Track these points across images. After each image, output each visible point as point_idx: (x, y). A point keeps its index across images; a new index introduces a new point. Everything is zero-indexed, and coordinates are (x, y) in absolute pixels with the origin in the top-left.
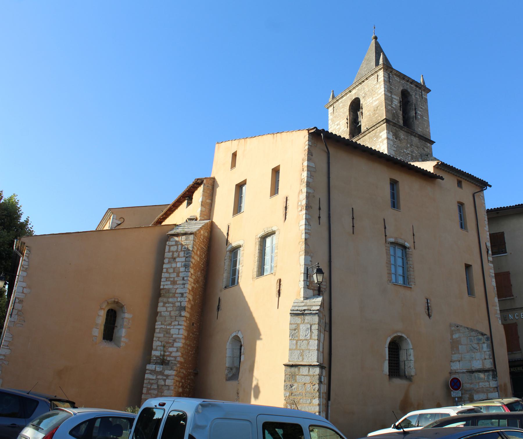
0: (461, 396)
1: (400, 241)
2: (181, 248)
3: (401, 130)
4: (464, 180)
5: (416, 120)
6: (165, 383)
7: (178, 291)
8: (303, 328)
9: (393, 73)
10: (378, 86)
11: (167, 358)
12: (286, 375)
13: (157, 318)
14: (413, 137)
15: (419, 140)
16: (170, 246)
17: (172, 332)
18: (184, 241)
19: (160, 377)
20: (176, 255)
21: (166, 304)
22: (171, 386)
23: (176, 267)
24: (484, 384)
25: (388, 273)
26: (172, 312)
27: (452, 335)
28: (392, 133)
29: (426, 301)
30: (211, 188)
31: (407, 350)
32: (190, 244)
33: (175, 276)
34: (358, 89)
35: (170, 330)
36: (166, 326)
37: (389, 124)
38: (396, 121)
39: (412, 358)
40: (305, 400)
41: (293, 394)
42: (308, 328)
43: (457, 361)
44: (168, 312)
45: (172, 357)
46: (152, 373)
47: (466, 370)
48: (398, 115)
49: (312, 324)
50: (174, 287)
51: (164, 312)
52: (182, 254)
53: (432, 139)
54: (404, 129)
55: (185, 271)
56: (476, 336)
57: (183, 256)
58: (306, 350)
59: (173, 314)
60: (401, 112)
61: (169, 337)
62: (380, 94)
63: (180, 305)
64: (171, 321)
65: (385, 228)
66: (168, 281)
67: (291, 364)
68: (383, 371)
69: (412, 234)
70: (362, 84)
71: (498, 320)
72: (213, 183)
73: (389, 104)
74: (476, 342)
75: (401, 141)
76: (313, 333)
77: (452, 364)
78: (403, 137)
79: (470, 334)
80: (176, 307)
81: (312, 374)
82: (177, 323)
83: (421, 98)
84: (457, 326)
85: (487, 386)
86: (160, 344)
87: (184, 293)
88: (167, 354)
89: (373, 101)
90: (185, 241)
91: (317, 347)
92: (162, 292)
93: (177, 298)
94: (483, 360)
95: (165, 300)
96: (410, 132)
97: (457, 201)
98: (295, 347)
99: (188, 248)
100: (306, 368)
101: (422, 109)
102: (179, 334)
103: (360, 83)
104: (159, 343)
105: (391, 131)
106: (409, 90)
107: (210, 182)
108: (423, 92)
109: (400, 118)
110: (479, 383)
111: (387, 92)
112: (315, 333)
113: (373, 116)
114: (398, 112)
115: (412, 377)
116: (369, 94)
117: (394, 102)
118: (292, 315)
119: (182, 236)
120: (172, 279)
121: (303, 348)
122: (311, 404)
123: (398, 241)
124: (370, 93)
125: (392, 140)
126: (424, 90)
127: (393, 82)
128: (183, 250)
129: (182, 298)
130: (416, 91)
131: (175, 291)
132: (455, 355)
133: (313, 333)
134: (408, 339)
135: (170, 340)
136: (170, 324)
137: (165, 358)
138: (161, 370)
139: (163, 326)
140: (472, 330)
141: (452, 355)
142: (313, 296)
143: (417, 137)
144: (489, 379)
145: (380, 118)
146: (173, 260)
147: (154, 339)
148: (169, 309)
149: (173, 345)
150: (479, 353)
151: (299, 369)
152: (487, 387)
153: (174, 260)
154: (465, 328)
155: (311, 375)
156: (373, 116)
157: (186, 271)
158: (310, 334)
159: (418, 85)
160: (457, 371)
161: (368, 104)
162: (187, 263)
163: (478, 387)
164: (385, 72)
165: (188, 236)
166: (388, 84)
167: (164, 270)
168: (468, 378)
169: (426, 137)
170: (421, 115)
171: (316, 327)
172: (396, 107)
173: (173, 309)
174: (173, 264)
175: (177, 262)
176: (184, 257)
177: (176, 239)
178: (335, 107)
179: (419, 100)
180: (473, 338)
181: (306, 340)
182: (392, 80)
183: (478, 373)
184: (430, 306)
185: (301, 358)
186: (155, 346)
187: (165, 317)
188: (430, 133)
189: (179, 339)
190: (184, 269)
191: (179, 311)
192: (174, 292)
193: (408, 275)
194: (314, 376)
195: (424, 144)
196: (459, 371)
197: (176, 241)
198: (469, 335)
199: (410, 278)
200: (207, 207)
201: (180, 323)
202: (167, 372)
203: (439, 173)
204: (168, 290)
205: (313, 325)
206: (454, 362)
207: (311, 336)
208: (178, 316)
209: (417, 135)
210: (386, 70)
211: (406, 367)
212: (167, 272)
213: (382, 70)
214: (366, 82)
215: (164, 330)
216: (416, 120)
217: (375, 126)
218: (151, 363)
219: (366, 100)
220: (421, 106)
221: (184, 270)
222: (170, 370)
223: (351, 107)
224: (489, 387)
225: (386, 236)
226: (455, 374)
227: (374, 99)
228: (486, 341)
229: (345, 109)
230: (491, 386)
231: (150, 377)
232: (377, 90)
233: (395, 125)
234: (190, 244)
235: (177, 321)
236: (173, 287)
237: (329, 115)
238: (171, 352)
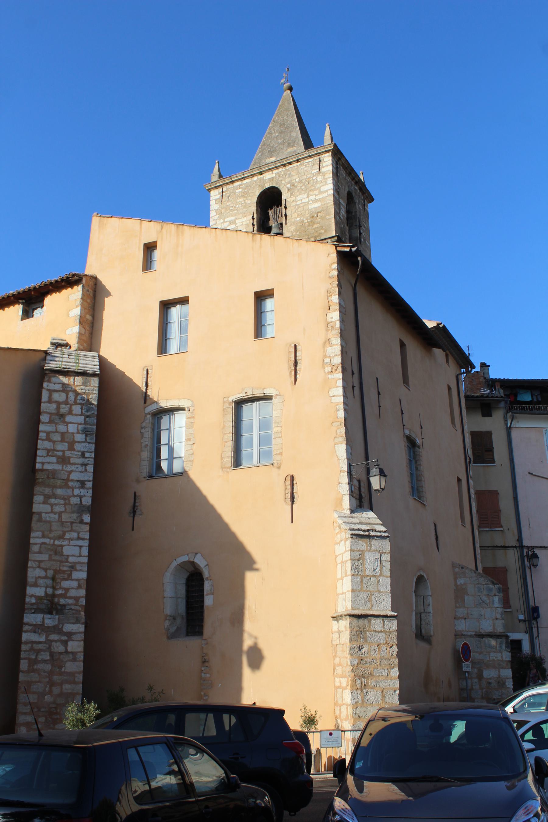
2: (75, 399)
6: (66, 648)
7: (73, 476)
8: (370, 557)
10: (320, 178)
11: (59, 600)
12: (351, 631)
13: (34, 525)
16: (51, 392)
17: (66, 551)
18: (79, 386)
19: (53, 637)
20: (64, 409)
21: (50, 500)
22: (79, 654)
23: (66, 431)
24: (496, 656)
26: (63, 514)
27: (455, 579)
30: (91, 295)
32: (93, 394)
33: (67, 449)
34: (278, 173)
35: (62, 549)
36: (52, 541)
40: (380, 671)
41: (363, 662)
43: (462, 618)
44: (55, 513)
45: (70, 598)
46: (37, 630)
47: (474, 633)
49: (382, 553)
50: (64, 469)
51: (46, 513)
52: (77, 409)
55: (86, 441)
56: (486, 584)
57: (80, 413)
58: (376, 592)
59: (65, 517)
61: (61, 562)
62: (324, 192)
63: (79, 503)
64: (63, 531)
66: (52, 456)
67: (360, 614)
70: (287, 167)
76: (384, 566)
80: (71, 506)
82: (75, 535)
84: (462, 568)
86: (42, 573)
87: (86, 481)
88: (59, 592)
89: (309, 201)
90: (81, 387)
91: (390, 588)
92: (39, 475)
93: (73, 489)
94: (494, 619)
95: (48, 491)
98: (360, 586)
99: (88, 400)
100: (380, 620)
102: (80, 556)
103: (283, 165)
104: (40, 573)
110: (489, 652)
112: (387, 566)
113: (309, 226)
116: (301, 187)
118: (354, 537)
119: (75, 376)
120: (60, 454)
121: (371, 588)
122: (389, 676)
124: (303, 187)
128: (78, 401)
129: (81, 490)
131: (66, 476)
133: (384, 566)
134: (428, 581)
135: (64, 566)
136: (61, 537)
137: (56, 600)
138: (56, 623)
139: (47, 541)
144: (502, 648)
145: (323, 231)
146: (58, 417)
147: (30, 564)
148: (57, 509)
149: (70, 575)
151: (370, 622)
152: (499, 660)
153: (60, 419)
154: (472, 572)
156: (309, 226)
157: (88, 441)
160: (464, 633)
161: (298, 203)
162: (89, 426)
165: (88, 378)
167: (42, 435)
168: (476, 645)
173: (66, 509)
174: (60, 426)
175: (68, 423)
176: (82, 414)
177: (64, 380)
178: (226, 191)
180: (481, 586)
181: (375, 576)
183: (489, 638)
185: (369, 605)
186: (32, 577)
187: (49, 522)
189: (81, 565)
190: (84, 437)
191: (78, 513)
192: (65, 477)
193: (417, 487)
194: (390, 632)
197: (64, 384)
199: (423, 491)
200: (87, 328)
201: (81, 536)
202: (68, 627)
204: (53, 474)
205: (383, 554)
207: (381, 570)
208: (75, 523)
212: (48, 439)
213: (331, 153)
214: (295, 165)
215: (49, 547)
218: (26, 611)
219: (293, 195)
221: (84, 440)
222: (74, 624)
227: (313, 197)
228: (498, 593)
229: (247, 200)
231: (34, 637)
232: (318, 185)
234: (93, 394)
235: (75, 531)
236: (63, 468)
237: (212, 203)
238: (67, 590)
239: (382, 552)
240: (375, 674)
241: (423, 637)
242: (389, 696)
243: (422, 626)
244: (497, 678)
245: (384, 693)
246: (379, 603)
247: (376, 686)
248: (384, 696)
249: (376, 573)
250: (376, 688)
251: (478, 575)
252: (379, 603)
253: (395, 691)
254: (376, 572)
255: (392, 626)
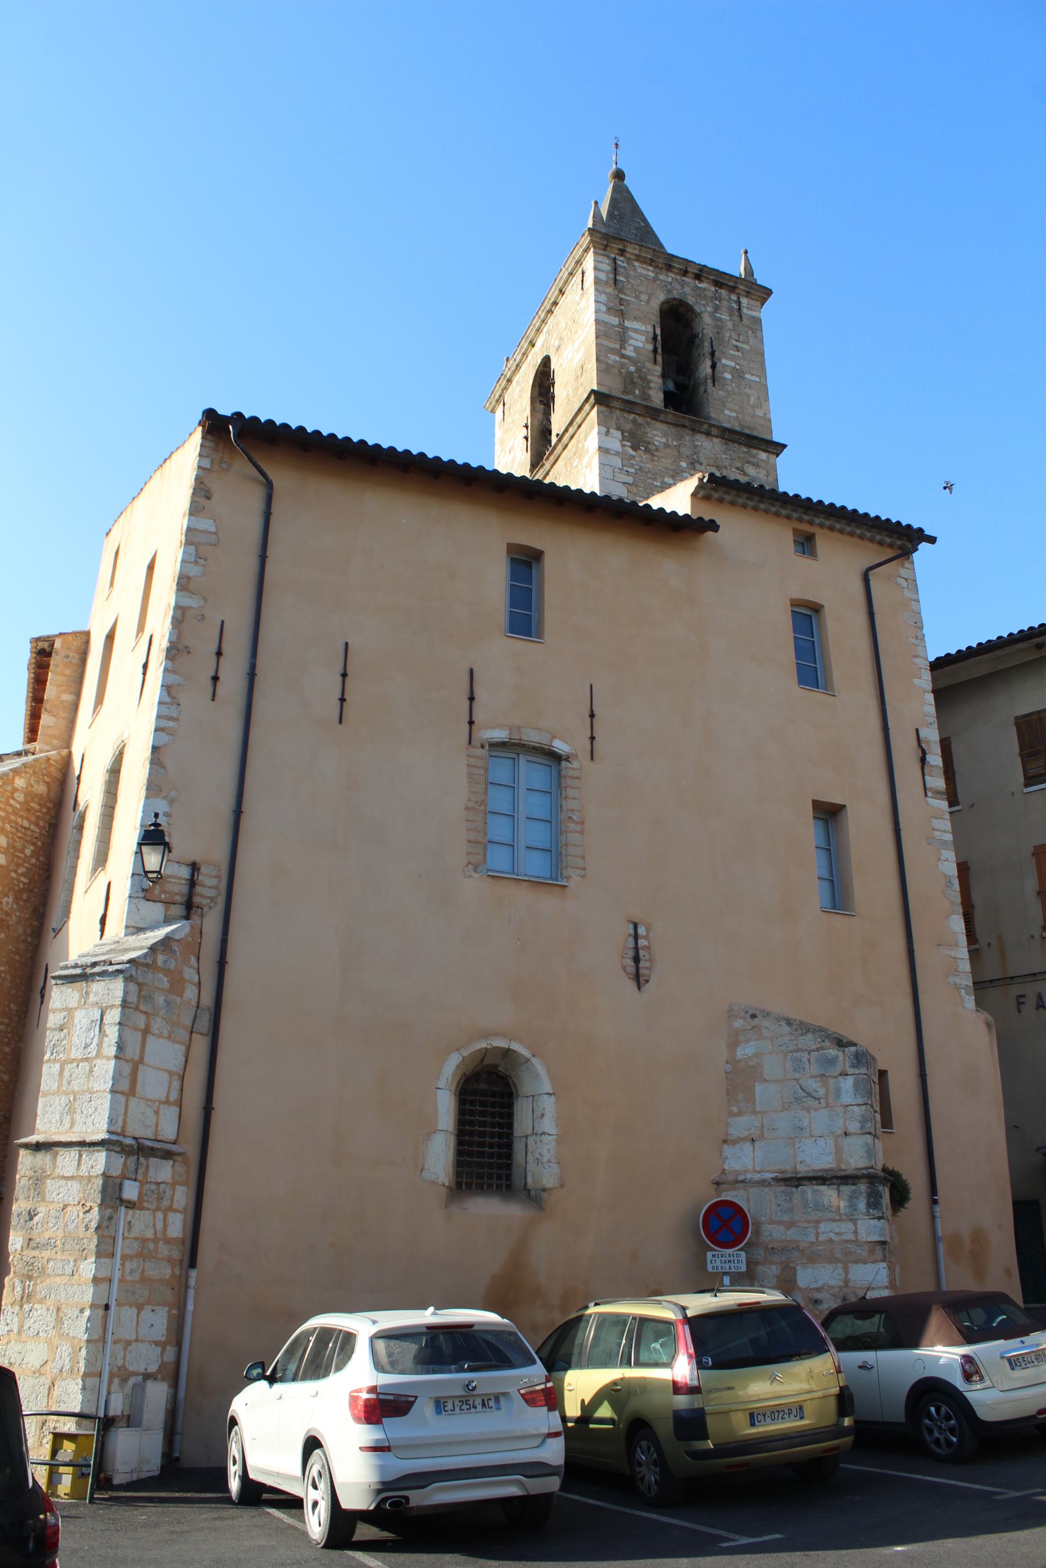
0: (744, 1269)
1: (532, 737)
3: (653, 422)
4: (825, 531)
5: (714, 385)
9: (628, 256)
14: (698, 436)
15: (726, 444)
24: (837, 1230)
25: (469, 841)
27: (733, 1045)
28: (620, 432)
29: (632, 931)
31: (535, 1098)
37: (607, 406)
38: (635, 396)
39: (548, 1125)
40: (60, 1265)
42: (93, 1021)
47: (773, 1175)
48: (644, 379)
53: (777, 438)
54: (663, 416)
56: (818, 1050)
60: (658, 369)
65: (472, 699)
68: (422, 1170)
69: (587, 713)
71: (961, 996)
72: (83, 647)
73: (612, 349)
74: (815, 1069)
75: (656, 453)
76: (107, 1036)
77: (727, 1150)
78: (664, 440)
79: (795, 1042)
81: (87, 1174)
83: (736, 318)
85: (845, 1237)
94: (839, 1136)
96: (686, 423)
97: (791, 600)
98: (57, 1084)
100: (74, 1153)
101: (738, 351)
105: (614, 426)
106: (691, 300)
107: (75, 643)
108: (744, 301)
109: (652, 385)
110: (818, 1222)
111: (606, 313)
114: (645, 370)
115: (545, 1194)
117: (631, 342)
121: (76, 1086)
122: (76, 1277)
123: (523, 738)
125: (617, 454)
126: (748, 292)
127: (632, 281)
130: (716, 299)
132: (739, 1119)
133: (107, 1036)
134: (533, 1060)
140: (805, 1028)
141: (732, 1120)
142: (165, 922)
143: (717, 437)
144: (856, 1210)
150: (825, 1112)
152: (847, 1241)
155: (82, 1177)
158: (99, 1038)
159: (721, 280)
160: (741, 1178)
163: (814, 1240)
164: (603, 255)
166: (610, 290)
169: (755, 433)
170: (734, 371)
171: (114, 1016)
172: (638, 353)
179: (730, 325)
181: (86, 1060)
182: (624, 277)
183: (816, 1185)
184: (648, 948)
188: (770, 421)
195: (746, 455)
196: (749, 1176)
198: (792, 1048)
203: (708, 513)
205: (108, 1011)
206: (734, 1142)
207: (100, 1045)
209: (714, 431)
210: (605, 250)
211: (530, 1159)
214: (562, 301)
216: (714, 385)
217: (575, 424)
220: (735, 343)
223: (537, 389)
224: (852, 1241)
225: (471, 723)
226: (734, 1189)
230: (863, 1236)
233: (629, 406)
239: (106, 1006)
240: (49, 1271)
241: (529, 1191)
242: (70, 1321)
243: (528, 1166)
244: (840, 1288)
245: (61, 1314)
246: (87, 1117)
247: (48, 1297)
248: (59, 1321)
249: (89, 1053)
250: (48, 1303)
251: (796, 1030)
252: (87, 1117)
253: (82, 1311)
254: (89, 1051)
255: (94, 1164)
